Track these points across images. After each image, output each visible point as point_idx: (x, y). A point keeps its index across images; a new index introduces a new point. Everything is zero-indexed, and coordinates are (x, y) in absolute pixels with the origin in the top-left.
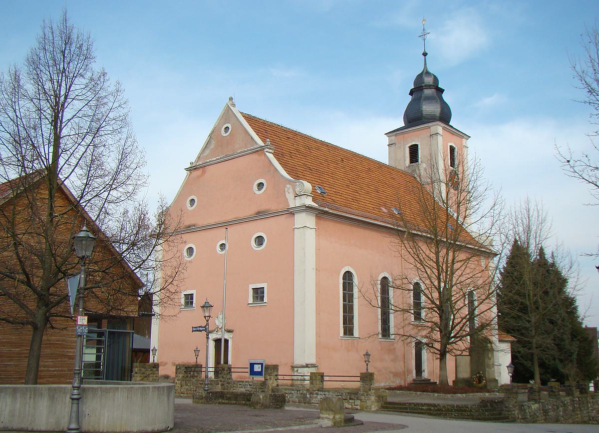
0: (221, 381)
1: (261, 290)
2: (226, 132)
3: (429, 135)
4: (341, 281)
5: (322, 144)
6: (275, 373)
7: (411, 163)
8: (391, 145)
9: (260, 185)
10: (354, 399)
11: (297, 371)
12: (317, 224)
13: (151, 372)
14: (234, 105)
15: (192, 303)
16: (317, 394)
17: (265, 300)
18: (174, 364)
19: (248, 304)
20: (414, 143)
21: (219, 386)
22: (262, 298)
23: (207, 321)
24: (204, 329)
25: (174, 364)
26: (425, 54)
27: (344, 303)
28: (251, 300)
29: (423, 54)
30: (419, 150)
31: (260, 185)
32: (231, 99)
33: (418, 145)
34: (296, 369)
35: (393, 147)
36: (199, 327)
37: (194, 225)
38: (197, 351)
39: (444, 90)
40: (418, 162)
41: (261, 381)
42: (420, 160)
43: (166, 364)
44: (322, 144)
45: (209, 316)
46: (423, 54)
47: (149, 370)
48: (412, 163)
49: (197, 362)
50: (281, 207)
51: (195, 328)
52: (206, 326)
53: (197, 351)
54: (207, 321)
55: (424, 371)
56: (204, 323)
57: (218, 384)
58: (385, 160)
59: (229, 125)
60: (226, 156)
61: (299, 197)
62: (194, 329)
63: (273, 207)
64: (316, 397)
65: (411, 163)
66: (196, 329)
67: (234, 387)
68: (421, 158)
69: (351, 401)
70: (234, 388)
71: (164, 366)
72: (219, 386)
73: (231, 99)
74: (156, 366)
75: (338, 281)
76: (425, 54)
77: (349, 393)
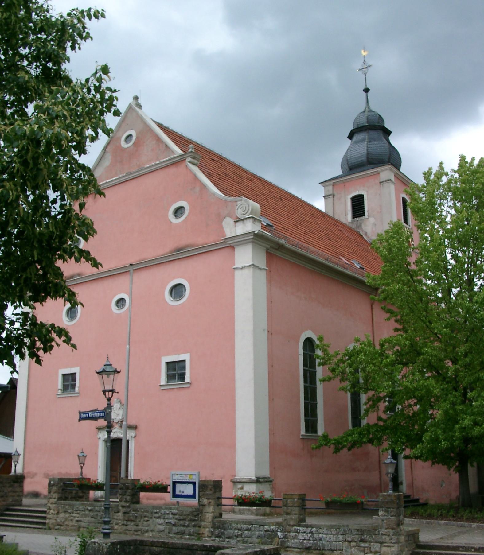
0: (123, 507)
1: (181, 364)
2: (130, 136)
3: (378, 182)
4: (301, 351)
5: (254, 177)
6: (217, 495)
7: (354, 218)
8: (327, 196)
9: (179, 211)
10: (370, 542)
11: (242, 488)
12: (269, 263)
13: (11, 489)
14: (140, 106)
15: (74, 386)
16: (297, 531)
17: (187, 379)
18: (46, 475)
19: (161, 385)
20: (357, 193)
21: (120, 514)
22: (182, 377)
23: (109, 399)
24: (103, 414)
25: (46, 475)
26: (367, 90)
27: (306, 385)
28: (163, 380)
29: (364, 91)
30: (365, 201)
31: (179, 211)
32: (136, 98)
33: (363, 195)
34: (239, 486)
35: (330, 199)
36: (94, 411)
37: (79, 275)
38: (82, 458)
39: (391, 132)
40: (364, 215)
41: (191, 507)
42: (366, 214)
43: (34, 475)
44: (254, 177)
45: (113, 391)
46: (364, 91)
47: (8, 485)
48: (356, 217)
49: (82, 474)
50: (212, 239)
51: (84, 413)
52: (105, 409)
53: (82, 458)
54: (109, 399)
55: (402, 483)
56: (102, 404)
57: (118, 512)
58: (323, 210)
59: (133, 133)
60: (128, 174)
61: (241, 223)
62: (83, 416)
63: (200, 240)
64: (295, 537)
65: (354, 218)
66: (85, 417)
67: (145, 517)
68: (368, 211)
69: (363, 545)
70: (146, 519)
71: (32, 478)
72: (120, 514)
73: (136, 98)
74: (20, 479)
75: (297, 351)
76: (367, 90)
77: (358, 530)
